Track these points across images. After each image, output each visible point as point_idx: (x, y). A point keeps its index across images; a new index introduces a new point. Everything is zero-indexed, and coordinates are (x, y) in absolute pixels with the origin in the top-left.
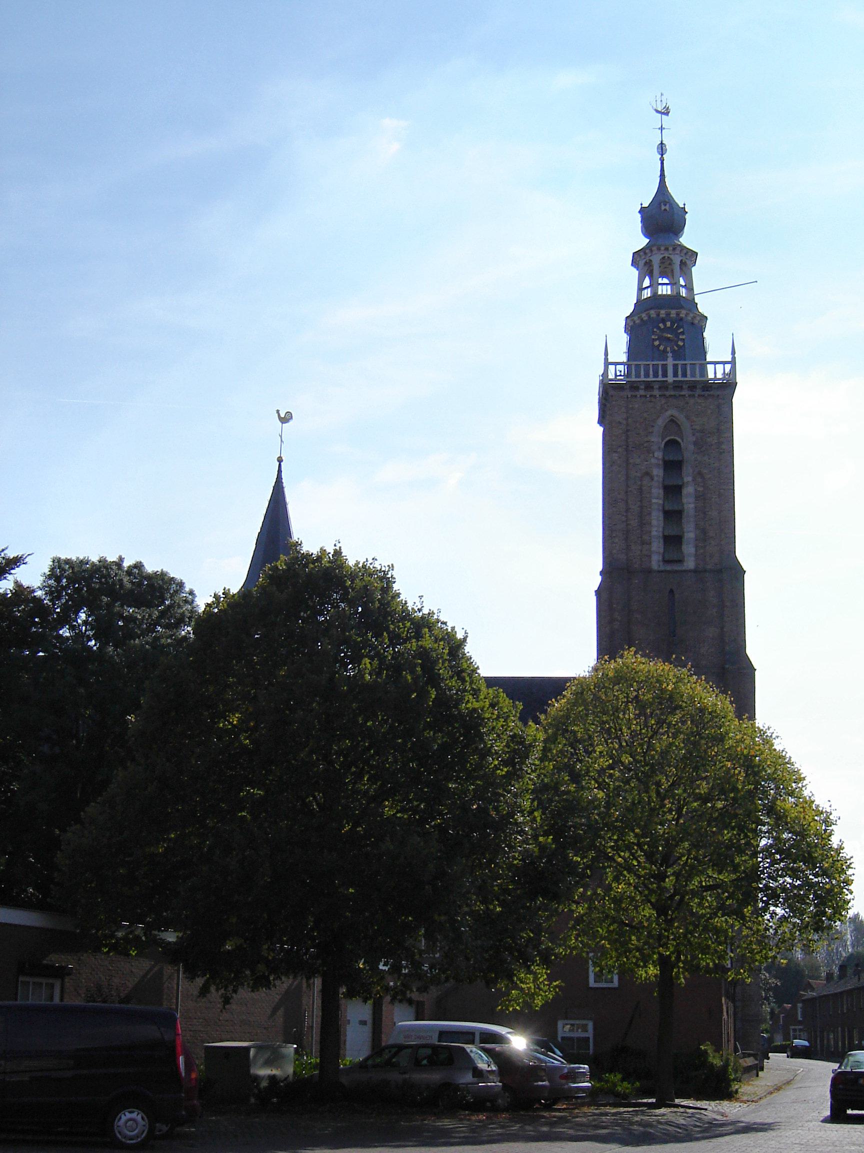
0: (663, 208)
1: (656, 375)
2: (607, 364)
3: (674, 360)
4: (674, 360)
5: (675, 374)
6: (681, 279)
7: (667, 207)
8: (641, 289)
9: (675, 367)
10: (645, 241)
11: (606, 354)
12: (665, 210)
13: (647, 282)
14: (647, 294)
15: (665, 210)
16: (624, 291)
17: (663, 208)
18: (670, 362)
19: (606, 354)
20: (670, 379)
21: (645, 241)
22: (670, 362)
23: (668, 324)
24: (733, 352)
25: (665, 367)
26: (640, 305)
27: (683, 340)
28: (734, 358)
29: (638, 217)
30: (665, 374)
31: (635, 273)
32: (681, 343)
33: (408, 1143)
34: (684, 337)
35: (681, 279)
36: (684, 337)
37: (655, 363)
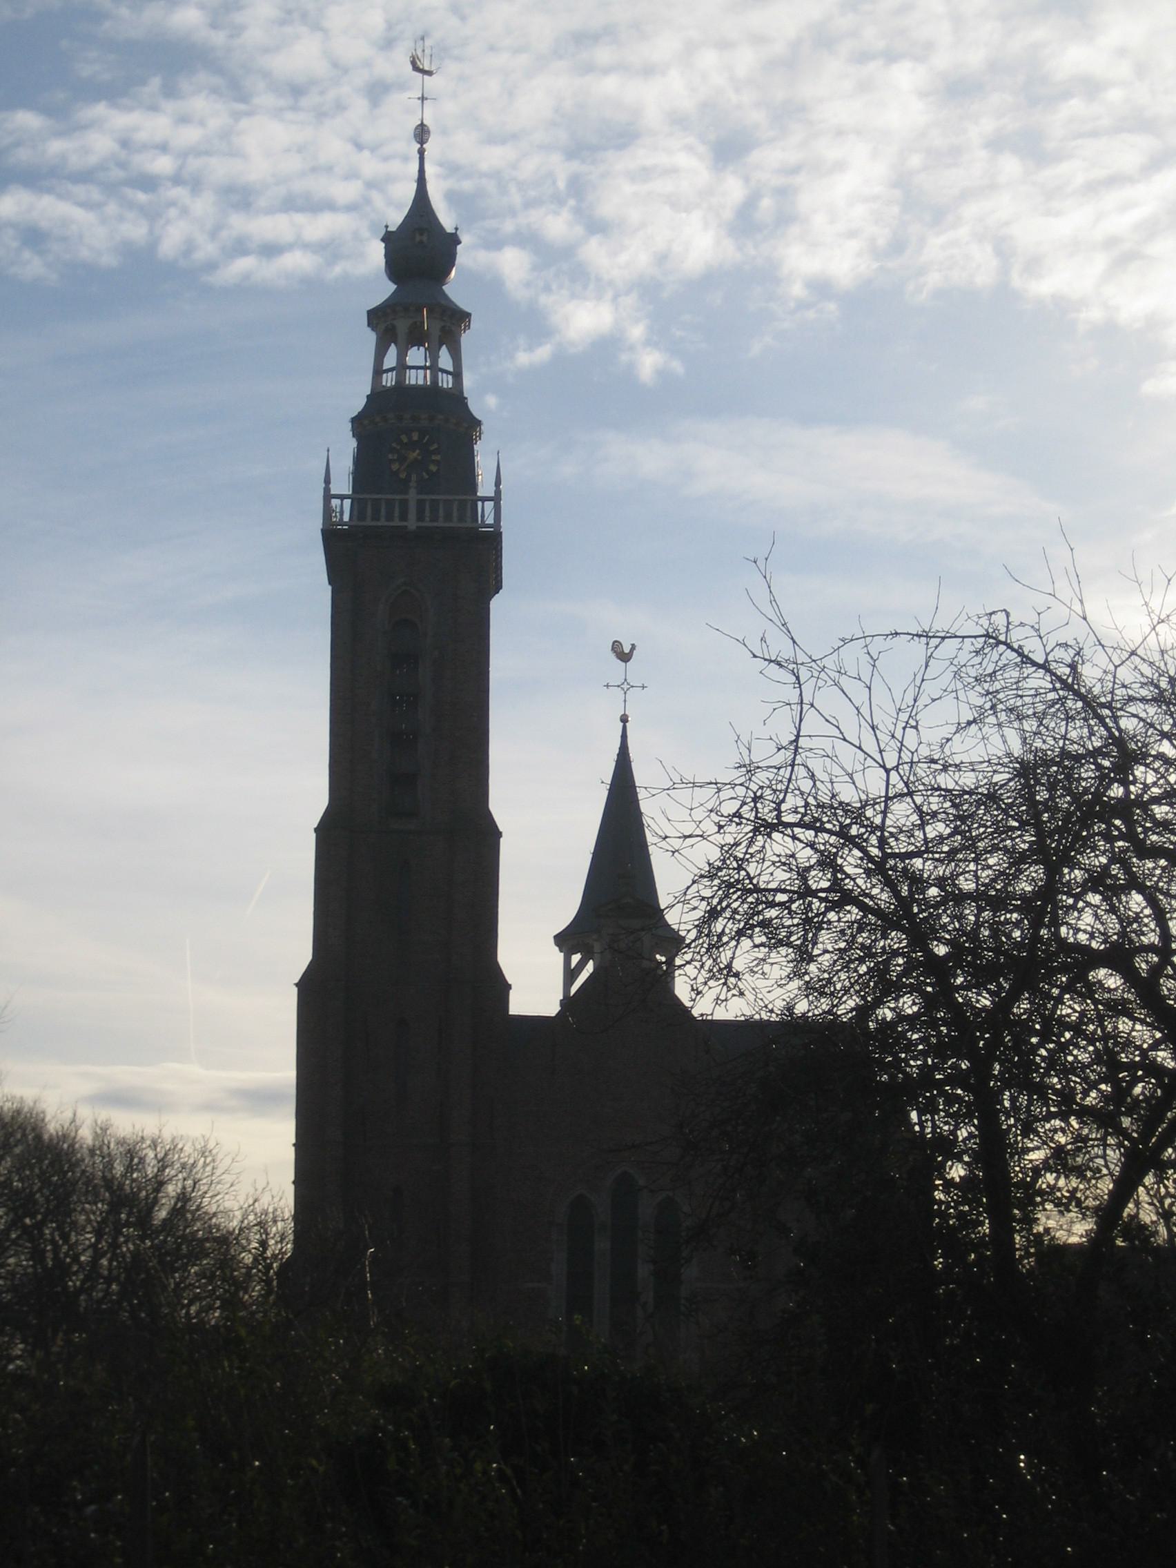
0: (418, 238)
1: (390, 517)
2: (328, 497)
3: (418, 493)
4: (418, 493)
5: (420, 517)
6: (658, 957)
7: (425, 238)
8: (378, 371)
9: (421, 503)
10: (392, 287)
11: (327, 481)
12: (421, 242)
13: (390, 360)
14: (389, 380)
15: (421, 242)
16: (346, 378)
17: (418, 238)
18: (412, 496)
19: (327, 481)
20: (412, 524)
21: (392, 287)
22: (412, 496)
23: (415, 437)
24: (498, 483)
25: (404, 503)
26: (377, 398)
27: (437, 463)
28: (498, 492)
29: (479, 418)
30: (404, 517)
31: (371, 338)
32: (433, 468)
33: (355, 513)
34: (438, 457)
35: (658, 957)
36: (438, 457)
37: (389, 497)
